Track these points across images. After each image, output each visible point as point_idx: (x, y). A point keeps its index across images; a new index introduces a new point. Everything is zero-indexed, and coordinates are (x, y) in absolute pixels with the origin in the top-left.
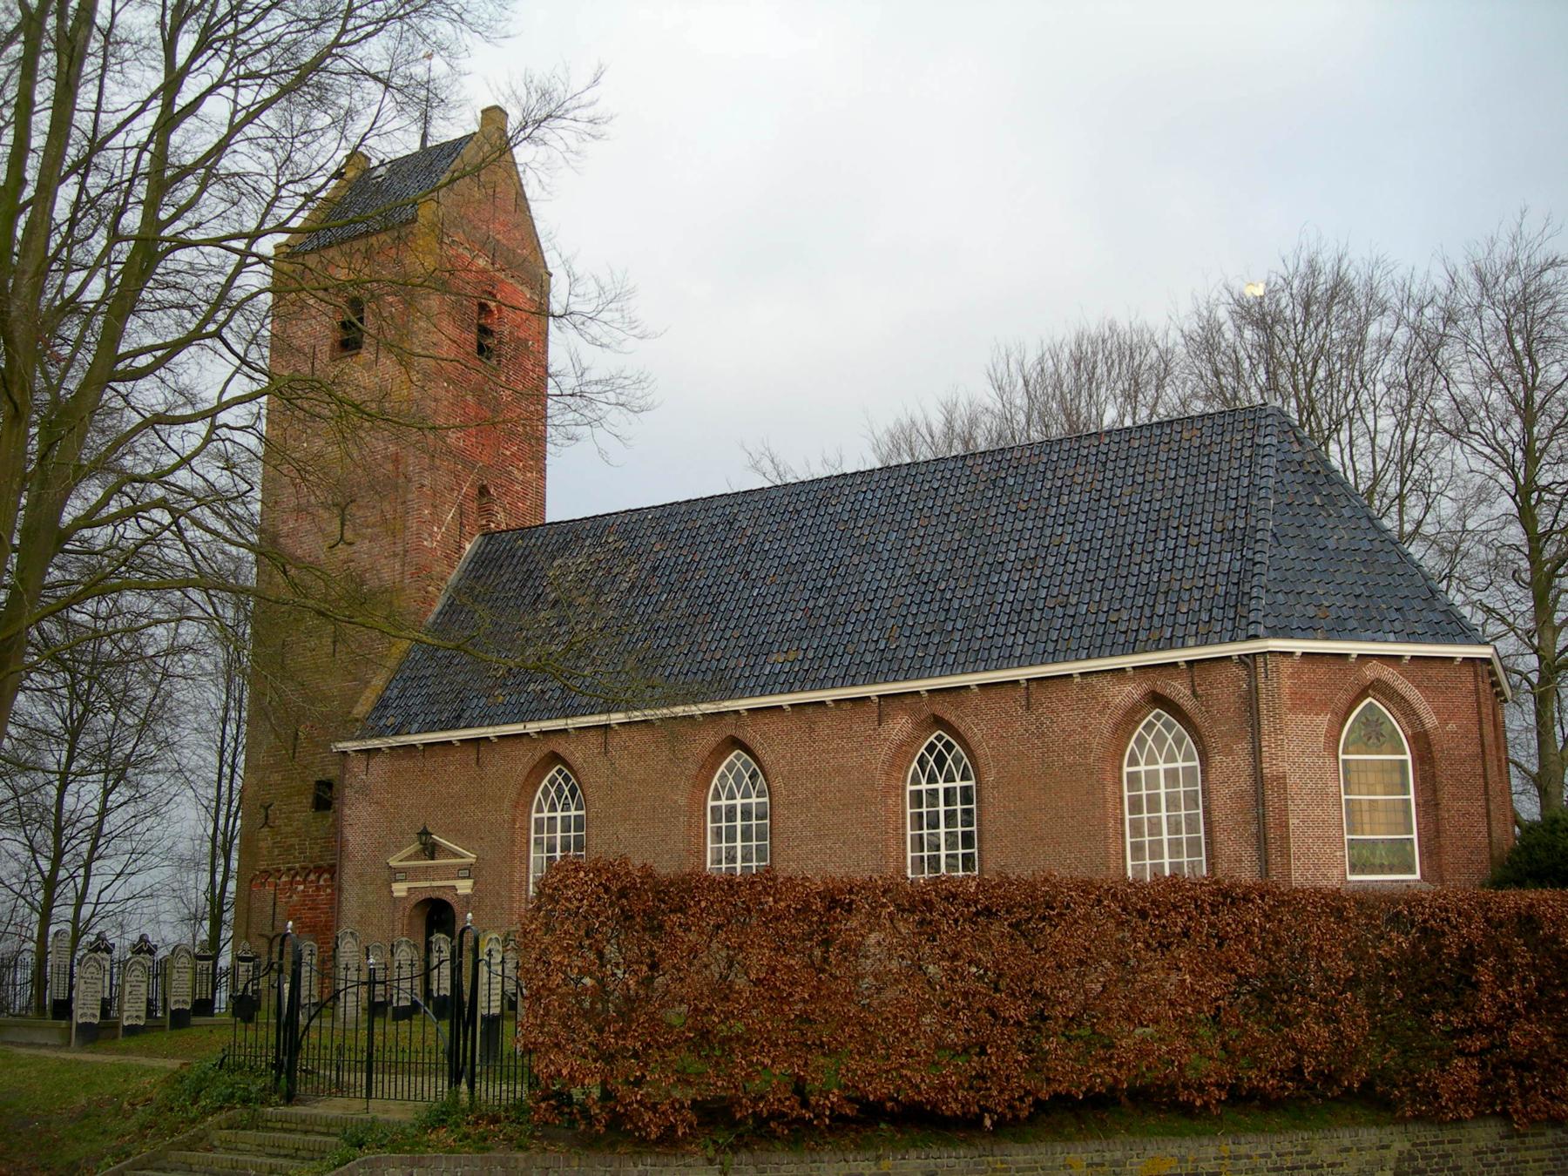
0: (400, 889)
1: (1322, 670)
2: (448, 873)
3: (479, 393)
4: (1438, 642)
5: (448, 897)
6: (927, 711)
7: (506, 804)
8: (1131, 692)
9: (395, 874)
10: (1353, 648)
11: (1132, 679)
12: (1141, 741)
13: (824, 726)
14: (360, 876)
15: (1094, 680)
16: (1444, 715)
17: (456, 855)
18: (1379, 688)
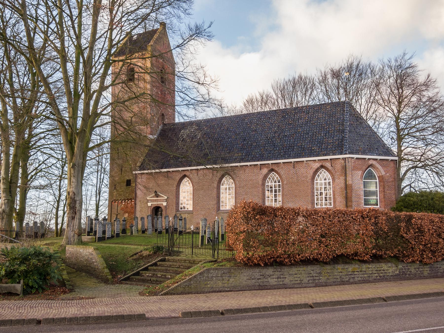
0: (149, 204)
1: (360, 162)
2: (161, 201)
3: (161, 91)
4: (385, 156)
5: (161, 206)
6: (271, 168)
7: (174, 186)
8: (317, 165)
9: (148, 201)
10: (367, 157)
11: (318, 162)
12: (318, 176)
13: (247, 170)
14: (140, 201)
15: (309, 162)
16: (386, 172)
17: (163, 197)
18: (371, 166)
